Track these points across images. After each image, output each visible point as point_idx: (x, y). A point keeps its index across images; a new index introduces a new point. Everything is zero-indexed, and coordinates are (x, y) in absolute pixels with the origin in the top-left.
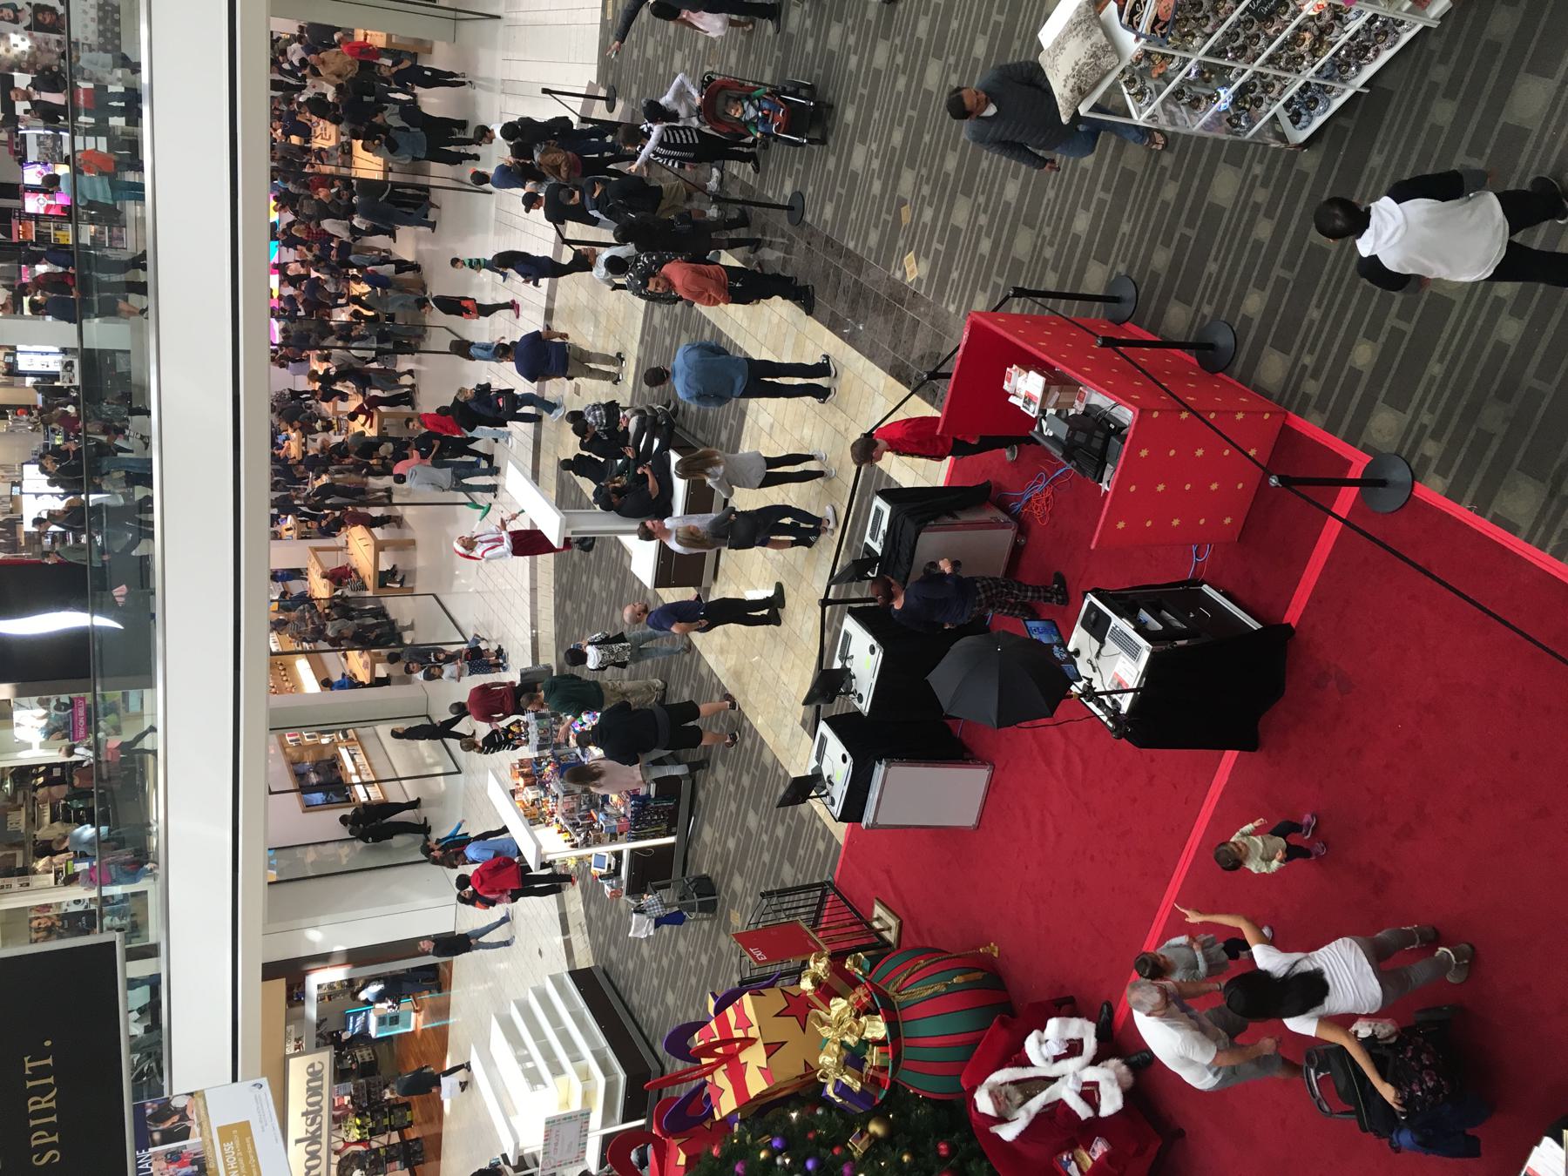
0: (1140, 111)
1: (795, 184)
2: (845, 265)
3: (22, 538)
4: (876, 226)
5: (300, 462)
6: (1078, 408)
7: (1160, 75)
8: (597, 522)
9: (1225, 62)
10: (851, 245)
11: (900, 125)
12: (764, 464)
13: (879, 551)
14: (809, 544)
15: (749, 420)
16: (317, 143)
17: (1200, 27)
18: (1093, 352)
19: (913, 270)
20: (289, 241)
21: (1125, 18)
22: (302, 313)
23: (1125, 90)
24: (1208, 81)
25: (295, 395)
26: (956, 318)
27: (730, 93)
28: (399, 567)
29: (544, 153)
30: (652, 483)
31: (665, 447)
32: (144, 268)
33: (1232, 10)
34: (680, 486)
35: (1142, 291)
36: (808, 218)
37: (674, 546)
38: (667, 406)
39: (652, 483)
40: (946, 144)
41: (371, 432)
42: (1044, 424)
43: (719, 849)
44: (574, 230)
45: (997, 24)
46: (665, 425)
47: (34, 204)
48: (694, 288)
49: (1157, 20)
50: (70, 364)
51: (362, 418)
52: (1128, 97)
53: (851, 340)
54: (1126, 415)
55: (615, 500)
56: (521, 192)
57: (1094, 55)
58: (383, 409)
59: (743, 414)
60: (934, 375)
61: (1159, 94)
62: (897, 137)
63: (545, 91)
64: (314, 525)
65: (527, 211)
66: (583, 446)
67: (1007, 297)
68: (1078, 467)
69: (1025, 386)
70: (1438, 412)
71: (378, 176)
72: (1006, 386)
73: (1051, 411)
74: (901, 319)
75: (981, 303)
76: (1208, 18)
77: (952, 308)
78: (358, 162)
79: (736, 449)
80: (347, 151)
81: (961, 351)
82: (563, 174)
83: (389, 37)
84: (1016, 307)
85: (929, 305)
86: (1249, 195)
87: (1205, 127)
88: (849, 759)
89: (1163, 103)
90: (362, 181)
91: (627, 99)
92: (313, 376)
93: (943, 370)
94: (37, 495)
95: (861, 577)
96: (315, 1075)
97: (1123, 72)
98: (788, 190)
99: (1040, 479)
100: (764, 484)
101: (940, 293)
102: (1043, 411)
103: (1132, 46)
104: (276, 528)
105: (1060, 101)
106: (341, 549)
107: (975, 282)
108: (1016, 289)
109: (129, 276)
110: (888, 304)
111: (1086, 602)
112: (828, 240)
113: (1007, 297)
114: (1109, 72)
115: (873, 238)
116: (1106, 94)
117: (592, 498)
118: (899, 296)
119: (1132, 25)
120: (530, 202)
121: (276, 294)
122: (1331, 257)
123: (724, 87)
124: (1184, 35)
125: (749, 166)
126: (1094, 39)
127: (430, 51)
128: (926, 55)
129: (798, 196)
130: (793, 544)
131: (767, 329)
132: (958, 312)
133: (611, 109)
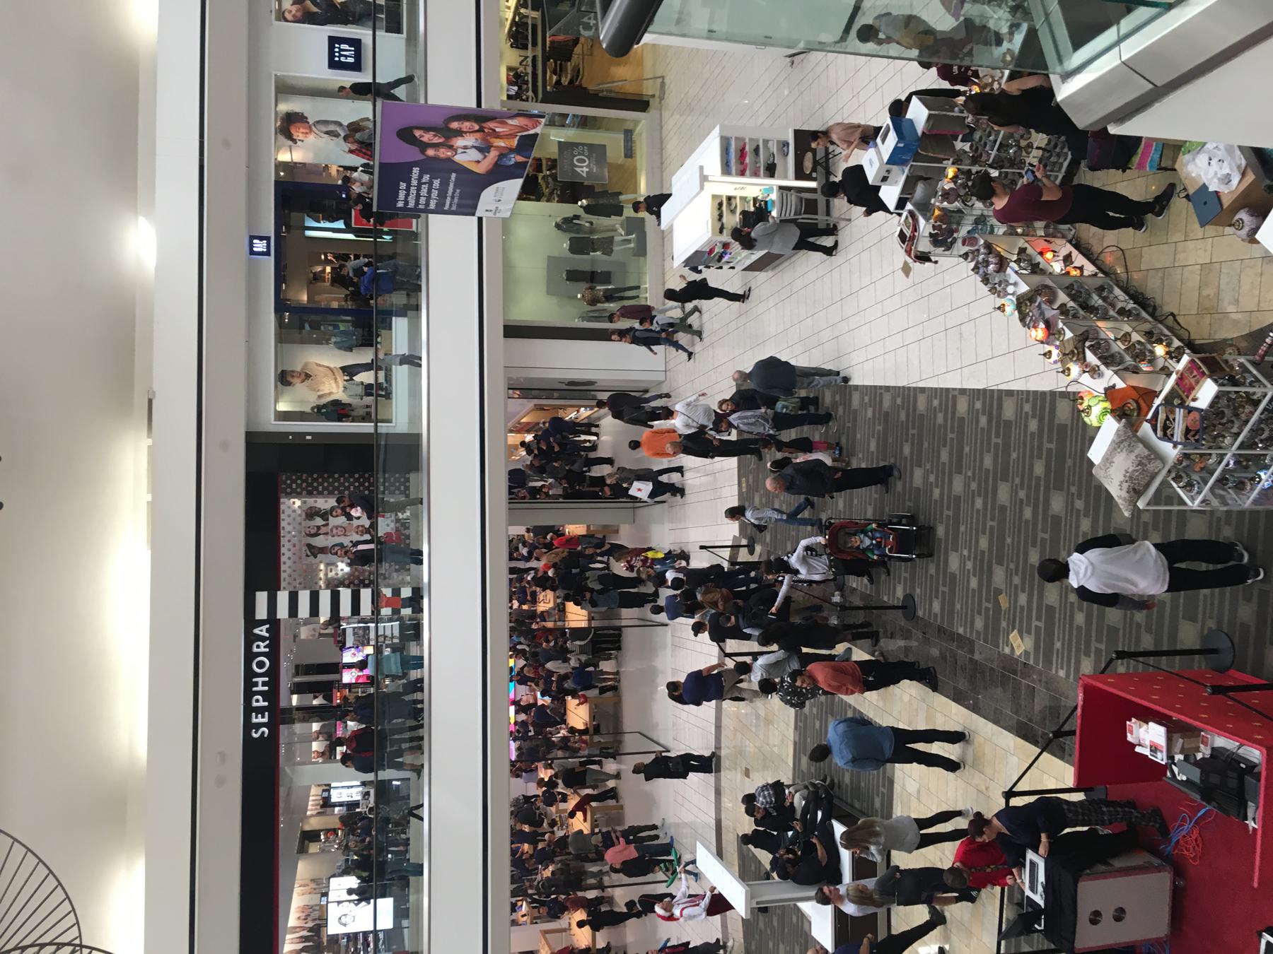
0: (1193, 499)
1: (905, 589)
2: (959, 647)
3: (325, 940)
4: (980, 613)
5: (532, 856)
6: (1204, 752)
7: (1202, 469)
8: (778, 891)
9: (1258, 451)
10: (961, 631)
11: (984, 533)
12: (916, 826)
13: (1042, 903)
14: (972, 900)
15: (897, 788)
16: (541, 607)
17: (1227, 430)
18: (1205, 699)
19: (1019, 645)
20: (521, 679)
21: (1160, 433)
22: (532, 733)
23: (1174, 485)
24: (1246, 467)
25: (527, 799)
26: (1070, 678)
27: (848, 530)
28: (613, 944)
29: (704, 594)
30: (820, 851)
31: (827, 818)
32: (422, 690)
33: (1252, 413)
34: (845, 856)
35: (1236, 640)
36: (920, 613)
37: (850, 909)
38: (824, 780)
39: (820, 851)
40: (1026, 542)
41: (586, 828)
42: (1176, 769)
44: (732, 645)
45: (1049, 450)
46: (827, 798)
47: (348, 677)
48: (833, 683)
49: (1187, 431)
50: (367, 794)
51: (579, 815)
52: (1179, 490)
53: (975, 709)
54: (1254, 754)
55: (790, 869)
56: (691, 621)
57: (1140, 463)
58: (594, 804)
59: (891, 782)
60: (1059, 734)
61: (1206, 484)
62: (984, 543)
63: (702, 547)
64: (544, 910)
65: (696, 635)
66: (757, 823)
67: (1111, 660)
68: (1220, 807)
69: (1148, 737)
71: (584, 624)
72: (1130, 738)
73: (1179, 757)
74: (1017, 686)
75: (1087, 667)
76: (1232, 422)
77: (1062, 673)
78: (570, 616)
79: (889, 815)
80: (561, 609)
81: (1079, 710)
82: (721, 607)
83: (588, 527)
84: (1121, 667)
85: (1040, 673)
87: (1255, 502)
89: (1211, 489)
90: (574, 630)
91: (764, 544)
92: (541, 783)
93: (1066, 728)
94: (339, 902)
95: (1029, 930)
97: (1169, 472)
98: (900, 593)
99: (1184, 819)
100: (920, 846)
101: (1048, 661)
102: (1171, 757)
103: (1171, 451)
104: (514, 916)
105: (1119, 501)
106: (564, 930)
107: (1078, 650)
108: (1118, 653)
109: (414, 734)
111: (1263, 943)
112: (941, 630)
113: (1111, 660)
114: (1157, 474)
115: (979, 623)
116: (1158, 491)
117: (768, 867)
118: (1010, 670)
119: (1167, 437)
120: (697, 629)
121: (512, 721)
123: (842, 527)
124: (1216, 437)
125: (865, 580)
126: (1137, 452)
127: (617, 532)
128: (995, 480)
129: (909, 598)
130: (957, 900)
131: (902, 706)
132: (1068, 676)
133: (751, 552)
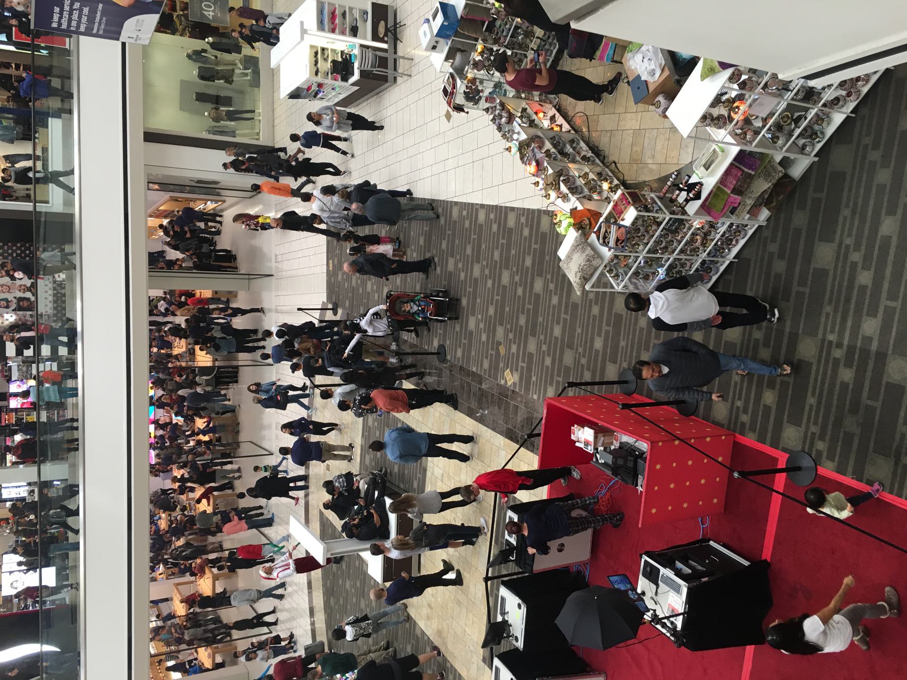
101: (527, 389)
110: (500, 399)
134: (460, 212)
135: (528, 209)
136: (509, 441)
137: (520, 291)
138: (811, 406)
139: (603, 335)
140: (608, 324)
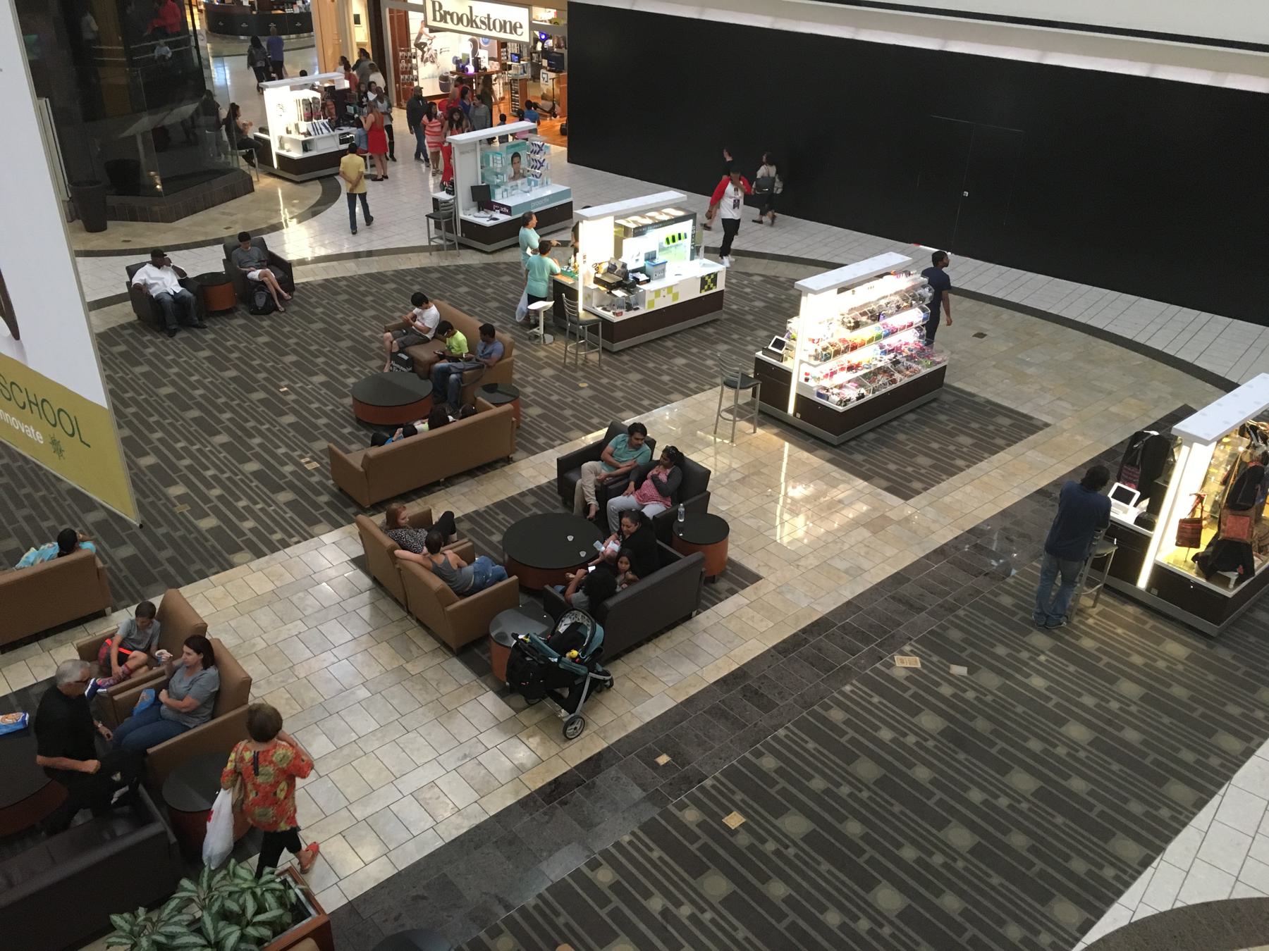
43: (530, 379)
70: (710, 925)
86: (1064, 743)
88: (841, 409)
96: (514, 29)
101: (867, 681)
110: (885, 632)
122: (934, 831)
134: (1221, 753)
135: (1177, 832)
136: (815, 618)
137: (1035, 745)
138: (892, 805)
139: (861, 843)
140: (1108, 665)
